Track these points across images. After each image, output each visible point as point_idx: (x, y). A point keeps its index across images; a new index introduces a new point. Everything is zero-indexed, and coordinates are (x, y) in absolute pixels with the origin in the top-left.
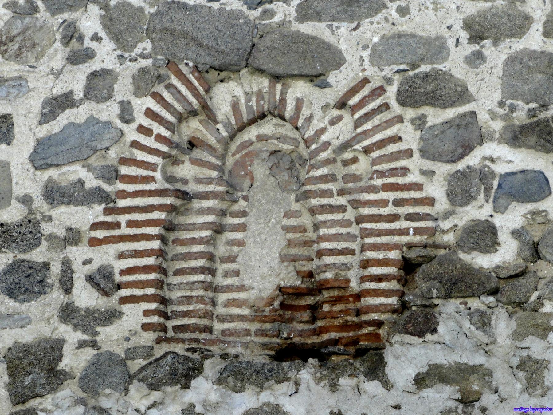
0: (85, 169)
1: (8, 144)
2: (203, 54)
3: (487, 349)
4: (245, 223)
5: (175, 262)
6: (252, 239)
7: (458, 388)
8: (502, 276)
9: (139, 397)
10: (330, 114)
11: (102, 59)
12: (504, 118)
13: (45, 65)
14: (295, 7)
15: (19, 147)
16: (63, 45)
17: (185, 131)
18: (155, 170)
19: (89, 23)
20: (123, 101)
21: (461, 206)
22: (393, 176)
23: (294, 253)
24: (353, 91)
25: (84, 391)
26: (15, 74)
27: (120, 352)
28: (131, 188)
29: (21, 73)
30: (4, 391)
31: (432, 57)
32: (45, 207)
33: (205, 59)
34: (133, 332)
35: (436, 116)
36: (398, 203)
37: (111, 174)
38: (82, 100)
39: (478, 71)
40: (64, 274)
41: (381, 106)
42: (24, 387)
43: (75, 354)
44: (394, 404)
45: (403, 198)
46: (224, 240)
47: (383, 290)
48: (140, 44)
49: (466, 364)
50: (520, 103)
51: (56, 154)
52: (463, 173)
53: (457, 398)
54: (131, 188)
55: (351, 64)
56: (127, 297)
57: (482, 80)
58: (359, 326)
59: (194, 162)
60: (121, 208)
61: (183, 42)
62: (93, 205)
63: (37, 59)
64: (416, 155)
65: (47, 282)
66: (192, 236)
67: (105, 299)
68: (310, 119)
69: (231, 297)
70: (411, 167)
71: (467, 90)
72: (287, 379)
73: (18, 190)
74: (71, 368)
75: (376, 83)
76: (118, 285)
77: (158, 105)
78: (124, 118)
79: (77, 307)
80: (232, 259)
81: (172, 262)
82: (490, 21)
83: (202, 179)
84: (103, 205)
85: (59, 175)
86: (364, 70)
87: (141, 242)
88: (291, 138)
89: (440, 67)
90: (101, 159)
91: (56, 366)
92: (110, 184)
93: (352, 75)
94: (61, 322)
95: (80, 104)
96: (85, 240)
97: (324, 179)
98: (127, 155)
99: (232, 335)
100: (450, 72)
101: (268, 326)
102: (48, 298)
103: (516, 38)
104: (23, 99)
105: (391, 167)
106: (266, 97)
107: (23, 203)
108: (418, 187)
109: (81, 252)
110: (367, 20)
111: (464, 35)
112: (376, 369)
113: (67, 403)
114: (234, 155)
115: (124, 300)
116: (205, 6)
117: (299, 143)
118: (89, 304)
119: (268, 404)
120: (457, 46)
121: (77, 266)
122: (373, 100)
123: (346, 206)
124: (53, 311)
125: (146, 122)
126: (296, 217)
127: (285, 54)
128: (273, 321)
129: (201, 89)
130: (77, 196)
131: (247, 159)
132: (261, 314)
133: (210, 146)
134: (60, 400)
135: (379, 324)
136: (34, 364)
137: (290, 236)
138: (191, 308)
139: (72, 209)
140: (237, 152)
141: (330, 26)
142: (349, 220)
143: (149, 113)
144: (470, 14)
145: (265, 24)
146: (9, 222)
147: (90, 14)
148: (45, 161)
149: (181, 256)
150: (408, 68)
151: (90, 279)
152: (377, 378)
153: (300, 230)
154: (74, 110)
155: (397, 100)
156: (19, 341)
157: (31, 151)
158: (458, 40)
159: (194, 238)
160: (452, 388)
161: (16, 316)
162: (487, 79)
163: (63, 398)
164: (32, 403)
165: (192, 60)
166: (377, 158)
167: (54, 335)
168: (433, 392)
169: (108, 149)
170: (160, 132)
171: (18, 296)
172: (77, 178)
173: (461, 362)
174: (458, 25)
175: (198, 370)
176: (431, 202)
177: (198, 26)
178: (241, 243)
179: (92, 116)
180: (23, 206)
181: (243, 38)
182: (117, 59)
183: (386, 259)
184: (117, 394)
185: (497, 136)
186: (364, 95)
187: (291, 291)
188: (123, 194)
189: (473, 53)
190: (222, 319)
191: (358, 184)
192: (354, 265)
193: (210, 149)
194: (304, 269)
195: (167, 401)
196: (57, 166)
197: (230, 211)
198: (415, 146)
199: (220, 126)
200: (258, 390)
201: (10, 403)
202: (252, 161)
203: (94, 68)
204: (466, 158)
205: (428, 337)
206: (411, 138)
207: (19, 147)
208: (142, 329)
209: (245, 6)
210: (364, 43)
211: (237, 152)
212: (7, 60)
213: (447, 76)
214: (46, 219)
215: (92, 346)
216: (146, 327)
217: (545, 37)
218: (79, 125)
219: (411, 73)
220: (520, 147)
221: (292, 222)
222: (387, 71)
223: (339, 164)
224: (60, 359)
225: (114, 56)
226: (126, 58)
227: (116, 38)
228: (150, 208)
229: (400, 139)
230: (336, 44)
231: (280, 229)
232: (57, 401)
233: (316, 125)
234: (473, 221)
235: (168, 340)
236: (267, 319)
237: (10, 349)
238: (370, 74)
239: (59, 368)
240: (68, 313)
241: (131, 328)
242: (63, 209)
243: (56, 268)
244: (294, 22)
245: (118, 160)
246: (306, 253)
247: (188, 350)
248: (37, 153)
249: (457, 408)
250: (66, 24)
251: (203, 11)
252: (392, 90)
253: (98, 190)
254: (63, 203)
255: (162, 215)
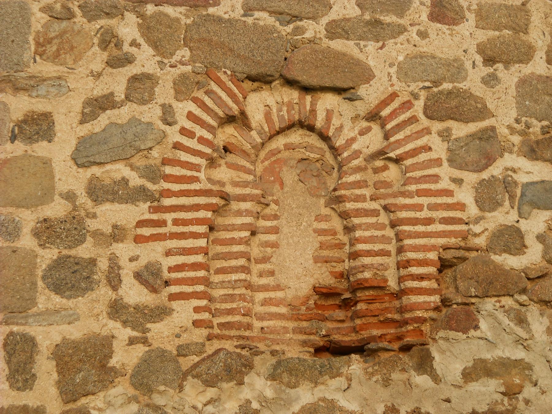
0: (128, 168)
1: (50, 142)
2: (240, 64)
3: (525, 344)
4: (277, 225)
5: (216, 261)
6: (285, 241)
7: (502, 381)
8: (531, 277)
9: (194, 394)
10: (360, 125)
11: (141, 63)
12: (523, 133)
13: (84, 67)
14: (324, 25)
15: (61, 145)
16: (101, 49)
17: (221, 136)
18: (199, 171)
19: (128, 30)
20: (165, 104)
21: (489, 212)
22: (426, 182)
23: (326, 255)
24: (385, 103)
25: (136, 388)
26: (55, 74)
27: (171, 348)
28: (176, 187)
29: (60, 74)
30: (53, 388)
31: (452, 76)
32: (89, 203)
33: (243, 68)
34: (183, 329)
35: (460, 130)
36: (432, 207)
37: (152, 174)
38: (123, 101)
39: (494, 90)
40: (111, 270)
41: (411, 118)
42: (75, 385)
43: (126, 351)
44: (443, 397)
45: (436, 203)
46: (258, 242)
47: (425, 288)
48: (178, 51)
49: (509, 358)
50: (534, 122)
51: (99, 153)
52: (489, 181)
53: (501, 391)
54: (176, 187)
55: (380, 79)
56: (175, 294)
57: (499, 98)
58: (406, 322)
59: (230, 166)
60: (166, 207)
61: (221, 52)
62: (138, 203)
63: (75, 61)
64: (445, 164)
65: (93, 278)
66: (231, 236)
67: (154, 295)
68: (340, 129)
69: (267, 296)
70: (442, 175)
71: (486, 107)
72: (339, 375)
73: (62, 187)
74: (123, 364)
75: (404, 97)
76: (166, 282)
77: (199, 110)
78: (166, 120)
79: (126, 303)
80: (265, 260)
81: (212, 261)
82: (499, 48)
83: (238, 182)
84: (148, 204)
85: (103, 172)
86: (392, 85)
87: (187, 240)
88: (317, 147)
89: (461, 85)
90: (143, 159)
91: (108, 363)
92: (154, 184)
93: (382, 89)
94: (110, 318)
95: (122, 106)
96: (130, 238)
97: (358, 185)
98: (169, 155)
99: (271, 332)
100: (471, 91)
101: (305, 324)
102: (92, 295)
103: (523, 63)
104: (63, 98)
105: (423, 174)
106: (296, 107)
107: (67, 199)
108: (448, 193)
109: (127, 249)
110: (392, 41)
111: (479, 59)
112: (425, 364)
113: (120, 401)
114: (263, 162)
115: (173, 297)
116: (240, 20)
117: (325, 152)
118: (138, 300)
119: (324, 399)
120: (474, 68)
121: (124, 261)
122: (403, 113)
123: (379, 211)
124: (102, 307)
125: (189, 125)
126: (326, 221)
127: (318, 67)
128: (310, 320)
129: (240, 96)
130: (122, 193)
131: (276, 166)
132: (298, 312)
133: (244, 151)
134: (112, 397)
135: (423, 321)
136: (85, 362)
137: (322, 238)
138: (234, 305)
139: (117, 206)
140: (266, 159)
141: (358, 45)
142: (383, 223)
143: (191, 116)
144: (482, 41)
145: (297, 39)
146: (53, 217)
147: (128, 22)
148: (88, 159)
149: (221, 256)
150: (432, 86)
151: (138, 276)
152: (425, 372)
153: (330, 233)
154: (116, 111)
155: (425, 113)
156: (68, 337)
157: (73, 149)
158: (474, 62)
159: (233, 238)
160: (497, 382)
161: (63, 312)
162: (503, 98)
163: (116, 395)
164: (83, 401)
165: (229, 68)
166: (410, 165)
167: (103, 331)
168: (479, 386)
169: (150, 149)
170: (202, 135)
171: (65, 292)
172: (120, 176)
173: (504, 357)
174: (473, 49)
175: (249, 366)
176: (461, 207)
177: (234, 38)
178: (275, 245)
179: (134, 117)
180: (67, 202)
181: (277, 51)
182: (157, 65)
183: (426, 259)
184: (172, 391)
185: (516, 149)
186: (394, 108)
187: (324, 291)
188: (169, 193)
189: (489, 75)
190: (261, 318)
191: (389, 191)
192: (391, 265)
193: (245, 154)
194: (337, 270)
195: (223, 397)
196: (100, 164)
197: (262, 214)
198: (444, 156)
199: (254, 133)
200: (313, 385)
201: (61, 401)
202: (281, 168)
203: (135, 72)
204: (490, 168)
205: (472, 333)
206: (440, 149)
207: (61, 145)
208: (193, 325)
209: (278, 22)
210: (390, 61)
211: (266, 159)
212: (45, 60)
213: (468, 95)
214: (91, 216)
215: (143, 343)
216: (196, 324)
217: (548, 64)
218: (121, 126)
219: (435, 90)
220: (537, 159)
221: (323, 226)
222: (414, 87)
223: (370, 171)
224: (109, 356)
225: (155, 61)
226: (166, 64)
227: (155, 45)
228: (196, 208)
229: (430, 149)
230: (364, 61)
231: (312, 232)
232: (109, 399)
233: (347, 135)
234: (501, 226)
235: (219, 337)
236: (304, 318)
237: (57, 345)
238: (398, 89)
239: (110, 365)
240: (116, 309)
241: (183, 324)
242: (107, 206)
243: (103, 264)
244: (324, 39)
245: (161, 160)
246: (336, 255)
247: (236, 347)
248: (79, 151)
249: (502, 400)
250: (102, 30)
251: (238, 25)
252: (419, 105)
253: (142, 190)
254: (108, 200)
255: (209, 214)
